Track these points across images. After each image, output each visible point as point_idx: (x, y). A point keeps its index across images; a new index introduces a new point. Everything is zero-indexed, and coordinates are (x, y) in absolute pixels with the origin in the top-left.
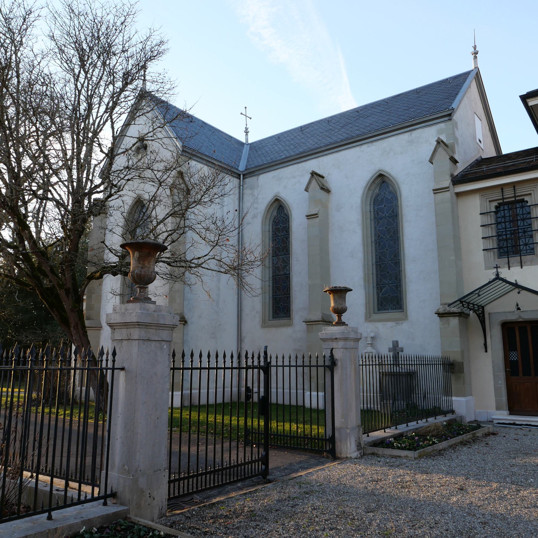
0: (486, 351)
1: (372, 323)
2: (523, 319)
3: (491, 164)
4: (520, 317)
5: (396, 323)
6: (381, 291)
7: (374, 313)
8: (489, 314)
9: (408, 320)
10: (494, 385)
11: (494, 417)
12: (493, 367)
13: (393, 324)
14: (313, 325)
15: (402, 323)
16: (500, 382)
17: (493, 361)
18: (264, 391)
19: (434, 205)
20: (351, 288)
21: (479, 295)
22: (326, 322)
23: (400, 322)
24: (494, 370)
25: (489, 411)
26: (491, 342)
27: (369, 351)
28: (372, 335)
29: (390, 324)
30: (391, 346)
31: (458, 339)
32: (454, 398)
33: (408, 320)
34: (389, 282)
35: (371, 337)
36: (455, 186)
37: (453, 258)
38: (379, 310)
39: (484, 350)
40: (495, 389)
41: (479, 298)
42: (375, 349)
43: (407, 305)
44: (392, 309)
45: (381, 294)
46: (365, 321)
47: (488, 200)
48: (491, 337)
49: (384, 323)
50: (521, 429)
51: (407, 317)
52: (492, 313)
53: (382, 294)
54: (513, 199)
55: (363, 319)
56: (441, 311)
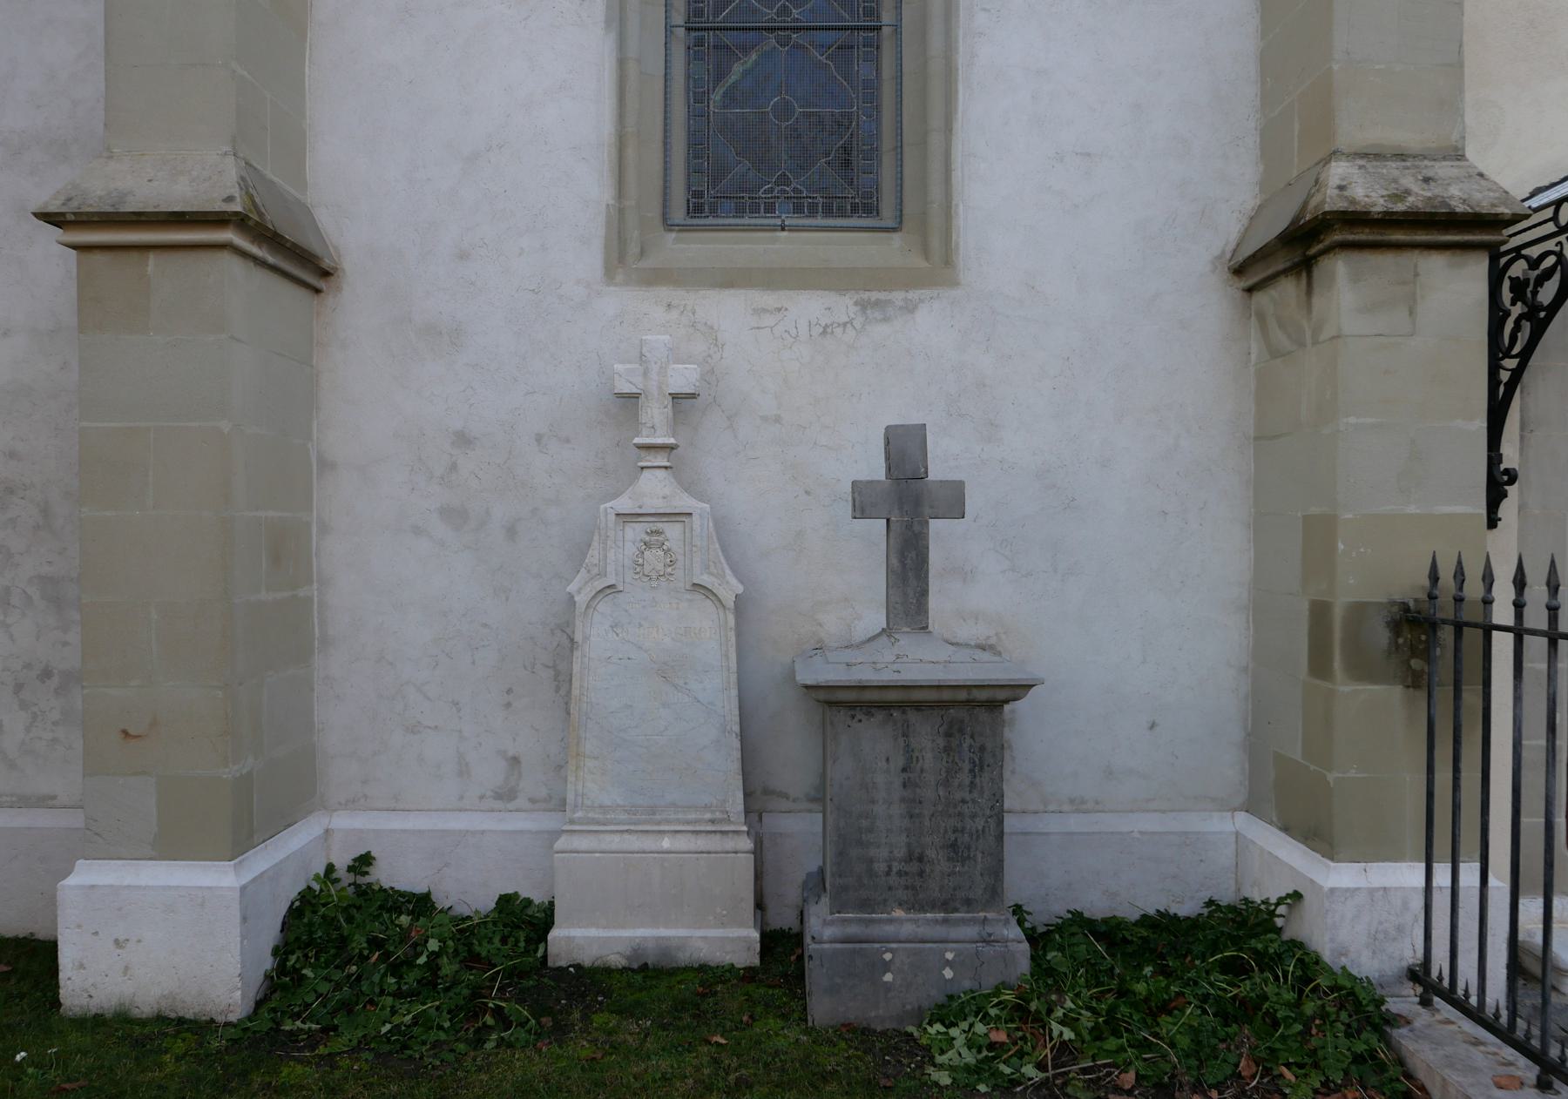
1: (665, 292)
5: (863, 306)
6: (720, 76)
7: (668, 225)
9: (954, 283)
13: (843, 306)
14: (152, 259)
15: (910, 308)
18: (1349, 241)
20: (33, 217)
22: (274, 240)
23: (898, 296)
27: (654, 504)
28: (683, 378)
29: (809, 307)
30: (874, 468)
33: (954, 283)
34: (784, 11)
35: (675, 397)
38: (695, 209)
42: (708, 502)
43: (957, 175)
44: (798, 209)
45: (717, 96)
46: (609, 273)
48: (1522, 428)
49: (768, 299)
51: (948, 260)
53: (730, 98)
55: (592, 260)
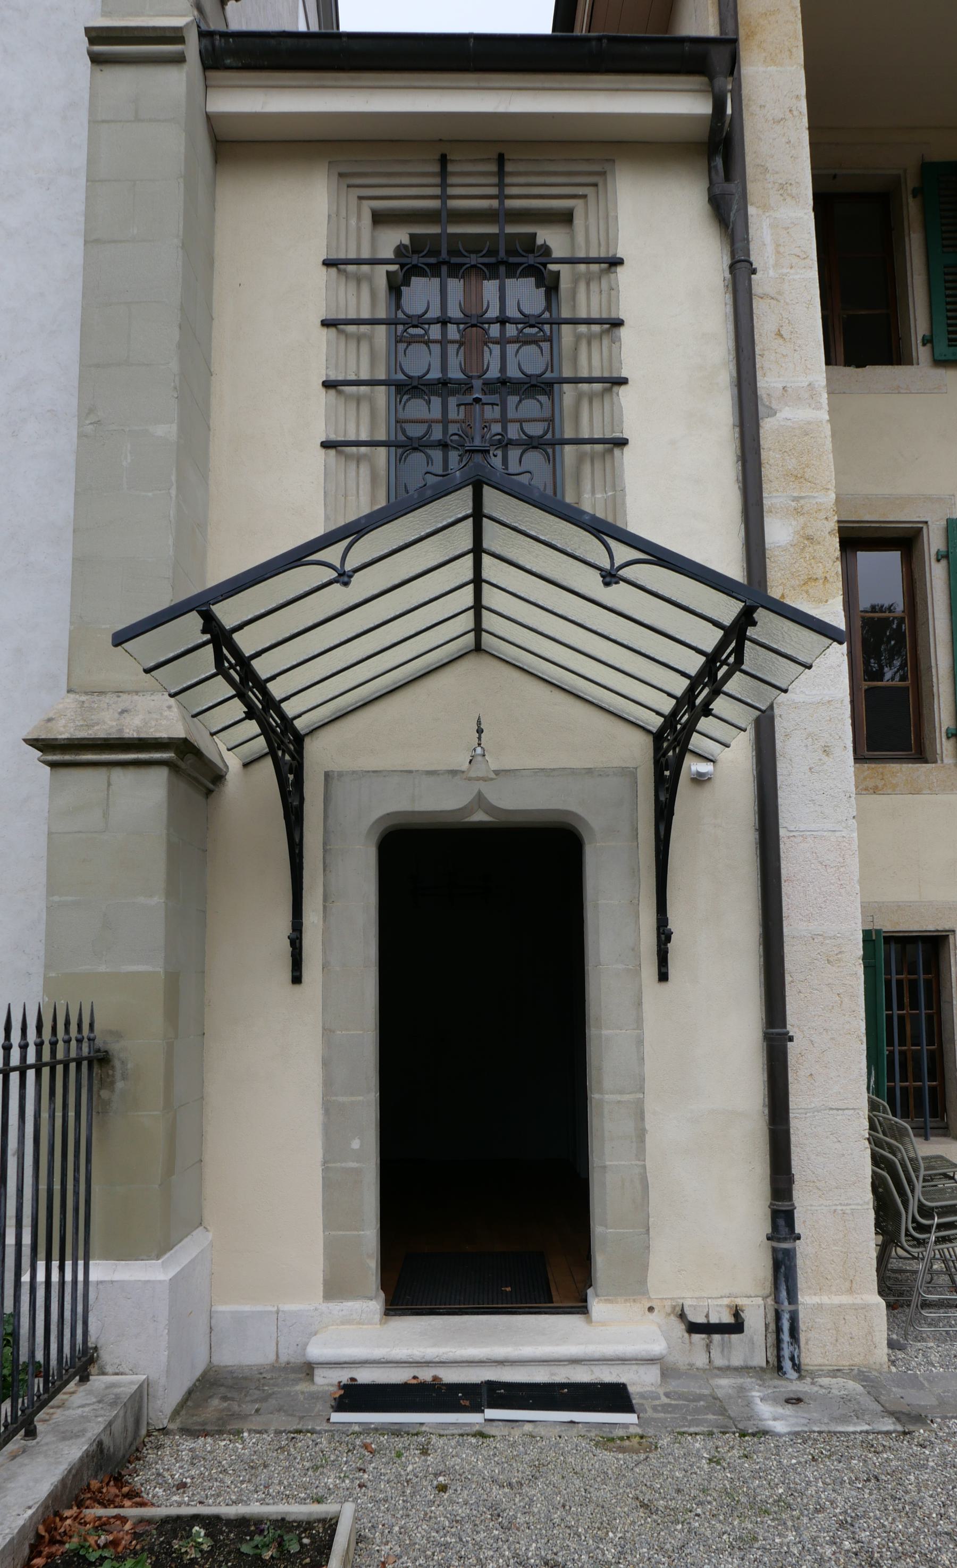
0: (297, 979)
2: (491, 809)
3: (15, 1334)
4: (480, 797)
8: (327, 776)
10: (325, 1162)
11: (316, 1351)
12: (326, 1063)
16: (356, 1144)
17: (327, 1032)
19: (83, 181)
21: (344, 578)
24: (328, 1083)
25: (288, 1307)
26: (326, 931)
31: (157, 900)
32: (99, 1271)
36: (214, 75)
37: (167, 430)
39: (287, 975)
40: (328, 1185)
41: (338, 597)
47: (367, 206)
48: (326, 898)
50: (481, 1435)
52: (341, 774)
54: (495, 203)
56: (64, 730)
